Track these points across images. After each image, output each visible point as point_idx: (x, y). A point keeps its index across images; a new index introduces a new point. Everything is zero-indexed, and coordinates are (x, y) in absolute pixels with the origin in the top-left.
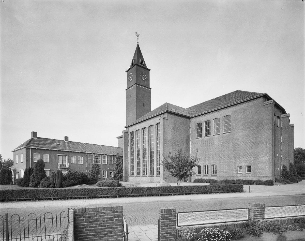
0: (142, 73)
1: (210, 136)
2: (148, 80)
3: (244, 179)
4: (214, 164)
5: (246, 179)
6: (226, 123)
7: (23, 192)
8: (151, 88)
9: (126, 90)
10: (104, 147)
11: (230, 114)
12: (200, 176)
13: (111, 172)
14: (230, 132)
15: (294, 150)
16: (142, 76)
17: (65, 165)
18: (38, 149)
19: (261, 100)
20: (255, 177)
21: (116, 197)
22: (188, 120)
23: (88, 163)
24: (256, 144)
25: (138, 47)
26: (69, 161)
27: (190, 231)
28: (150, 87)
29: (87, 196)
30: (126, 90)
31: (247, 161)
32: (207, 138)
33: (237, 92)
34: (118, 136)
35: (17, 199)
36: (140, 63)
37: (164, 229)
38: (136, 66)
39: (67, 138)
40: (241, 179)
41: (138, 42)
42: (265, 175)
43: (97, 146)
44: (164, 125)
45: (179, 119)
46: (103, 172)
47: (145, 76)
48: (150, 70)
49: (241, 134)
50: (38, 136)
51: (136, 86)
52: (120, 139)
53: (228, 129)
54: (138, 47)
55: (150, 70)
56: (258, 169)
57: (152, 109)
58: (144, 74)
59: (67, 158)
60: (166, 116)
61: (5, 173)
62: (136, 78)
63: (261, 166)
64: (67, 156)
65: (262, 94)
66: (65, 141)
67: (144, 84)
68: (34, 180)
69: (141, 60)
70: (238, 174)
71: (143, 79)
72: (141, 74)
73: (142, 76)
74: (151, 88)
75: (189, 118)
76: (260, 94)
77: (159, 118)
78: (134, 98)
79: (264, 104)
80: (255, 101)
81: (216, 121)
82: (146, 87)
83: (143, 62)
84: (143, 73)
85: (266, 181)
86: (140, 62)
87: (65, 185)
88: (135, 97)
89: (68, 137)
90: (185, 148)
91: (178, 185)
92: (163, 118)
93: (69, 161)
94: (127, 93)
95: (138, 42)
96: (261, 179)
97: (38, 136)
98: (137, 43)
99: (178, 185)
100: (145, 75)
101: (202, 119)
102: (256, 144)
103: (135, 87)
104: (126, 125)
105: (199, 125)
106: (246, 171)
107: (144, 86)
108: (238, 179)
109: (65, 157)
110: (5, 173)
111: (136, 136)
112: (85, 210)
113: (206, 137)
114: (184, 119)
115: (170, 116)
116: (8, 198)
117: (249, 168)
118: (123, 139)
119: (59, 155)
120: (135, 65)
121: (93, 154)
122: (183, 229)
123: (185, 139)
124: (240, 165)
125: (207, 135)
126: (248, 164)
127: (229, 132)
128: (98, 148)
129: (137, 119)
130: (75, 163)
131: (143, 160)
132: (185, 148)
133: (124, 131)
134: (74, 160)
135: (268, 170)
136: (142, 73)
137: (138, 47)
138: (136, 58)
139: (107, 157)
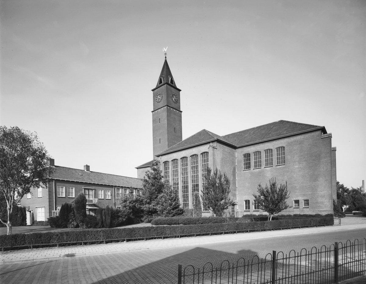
1: (261, 168)
2: (178, 101)
3: (301, 214)
4: (247, 199)
5: (304, 214)
6: (279, 154)
7: (150, 230)
8: (181, 112)
9: (152, 112)
10: (115, 177)
11: (284, 145)
12: (249, 211)
14: (285, 165)
17: (92, 201)
18: (63, 180)
19: (318, 133)
20: (314, 211)
21: (235, 232)
23: (116, 198)
24: (314, 178)
26: (96, 196)
29: (195, 234)
30: (152, 112)
31: (304, 195)
32: (257, 170)
33: (282, 122)
34: (137, 166)
35: (83, 242)
39: (88, 167)
40: (298, 213)
41: (166, 58)
42: (324, 209)
43: (115, 177)
44: (214, 155)
45: (226, 149)
48: (180, 90)
49: (297, 167)
50: (55, 164)
51: (167, 108)
53: (282, 161)
54: (166, 64)
56: (317, 203)
59: (94, 191)
60: (215, 144)
61: (18, 211)
62: (166, 98)
63: (320, 200)
64: (93, 189)
65: (319, 126)
66: (86, 170)
67: (173, 105)
68: (75, 219)
70: (294, 208)
76: (316, 126)
77: (208, 146)
78: (165, 122)
79: (322, 137)
80: (313, 134)
81: (268, 153)
82: (177, 110)
85: (326, 215)
87: (115, 224)
88: (166, 120)
89: (89, 166)
92: (213, 148)
93: (96, 196)
94: (153, 114)
95: (166, 58)
96: (320, 213)
97: (55, 164)
101: (251, 150)
102: (314, 178)
105: (247, 156)
106: (254, 208)
107: (175, 109)
108: (295, 213)
109: (91, 190)
110: (18, 211)
111: (171, 166)
112: (89, 258)
113: (256, 170)
115: (218, 144)
116: (135, 237)
117: (307, 202)
119: (85, 189)
120: (165, 84)
121: (121, 187)
123: (232, 170)
124: (297, 199)
125: (246, 169)
126: (306, 198)
127: (283, 165)
128: (123, 180)
129: (169, 146)
130: (101, 198)
134: (101, 194)
135: (328, 204)
139: (135, 191)
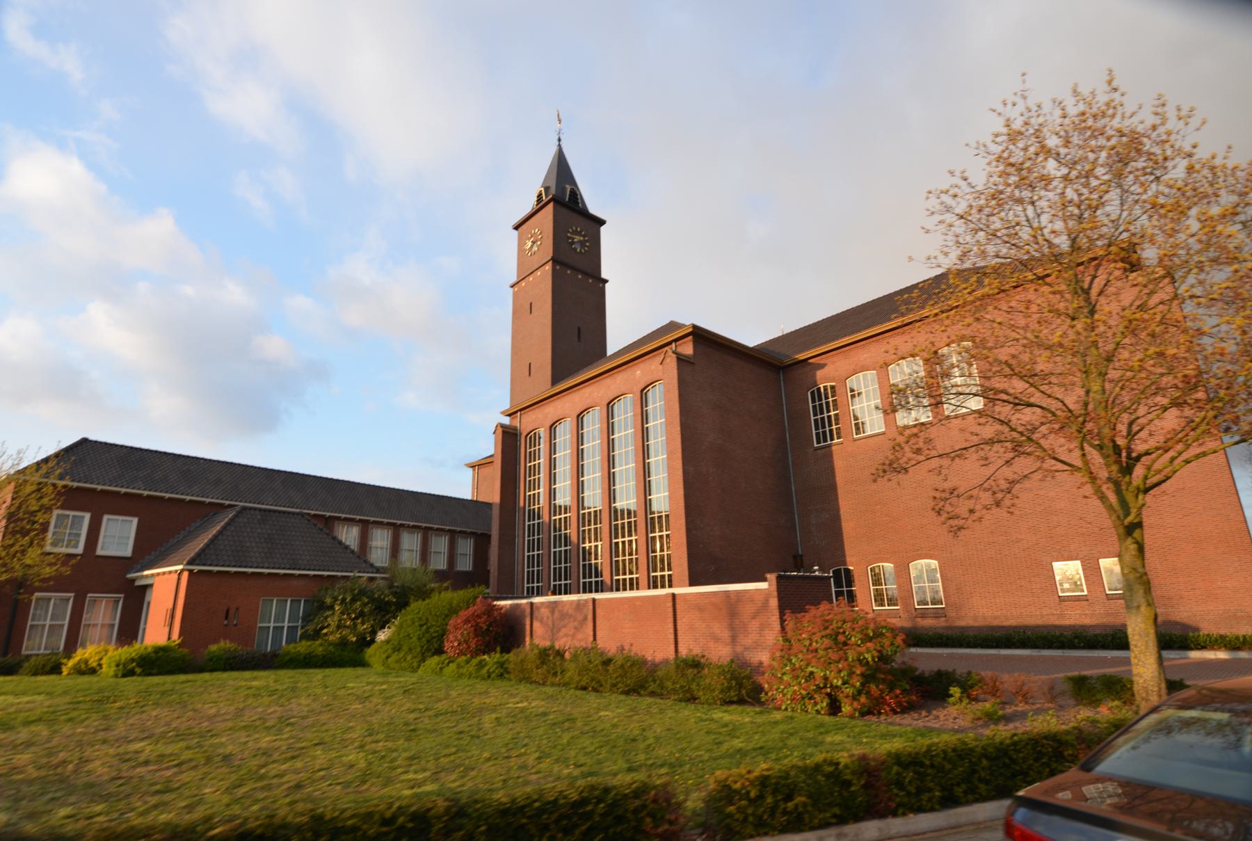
15: (897, 427)
27: (1102, 423)
38: (551, 205)
41: (559, 140)
51: (554, 269)
52: (486, 471)
55: (602, 222)
57: (611, 349)
71: (575, 249)
72: (569, 232)
83: (575, 195)
91: (683, 651)
94: (515, 295)
95: (559, 140)
99: (683, 651)
103: (550, 272)
104: (506, 405)
118: (496, 471)
122: (1119, 335)
131: (584, 583)
133: (503, 426)
138: (553, 185)
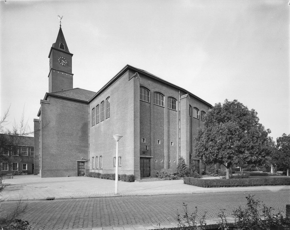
0: (60, 58)
13: (16, 164)
16: (61, 62)
22: (86, 105)
25: (61, 32)
28: (73, 73)
36: (59, 47)
37: (163, 102)
41: (61, 25)
46: (31, 154)
47: (65, 61)
48: (72, 55)
58: (63, 59)
69: (60, 44)
73: (61, 61)
74: (73, 75)
75: (88, 103)
82: (66, 73)
84: (62, 57)
86: (60, 45)
90: (79, 137)
95: (61, 25)
98: (60, 27)
100: (64, 60)
107: (64, 72)
114: (78, 104)
132: (79, 137)
136: (59, 59)
137: (61, 32)
